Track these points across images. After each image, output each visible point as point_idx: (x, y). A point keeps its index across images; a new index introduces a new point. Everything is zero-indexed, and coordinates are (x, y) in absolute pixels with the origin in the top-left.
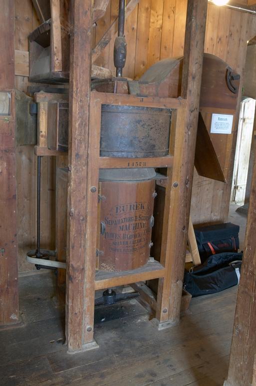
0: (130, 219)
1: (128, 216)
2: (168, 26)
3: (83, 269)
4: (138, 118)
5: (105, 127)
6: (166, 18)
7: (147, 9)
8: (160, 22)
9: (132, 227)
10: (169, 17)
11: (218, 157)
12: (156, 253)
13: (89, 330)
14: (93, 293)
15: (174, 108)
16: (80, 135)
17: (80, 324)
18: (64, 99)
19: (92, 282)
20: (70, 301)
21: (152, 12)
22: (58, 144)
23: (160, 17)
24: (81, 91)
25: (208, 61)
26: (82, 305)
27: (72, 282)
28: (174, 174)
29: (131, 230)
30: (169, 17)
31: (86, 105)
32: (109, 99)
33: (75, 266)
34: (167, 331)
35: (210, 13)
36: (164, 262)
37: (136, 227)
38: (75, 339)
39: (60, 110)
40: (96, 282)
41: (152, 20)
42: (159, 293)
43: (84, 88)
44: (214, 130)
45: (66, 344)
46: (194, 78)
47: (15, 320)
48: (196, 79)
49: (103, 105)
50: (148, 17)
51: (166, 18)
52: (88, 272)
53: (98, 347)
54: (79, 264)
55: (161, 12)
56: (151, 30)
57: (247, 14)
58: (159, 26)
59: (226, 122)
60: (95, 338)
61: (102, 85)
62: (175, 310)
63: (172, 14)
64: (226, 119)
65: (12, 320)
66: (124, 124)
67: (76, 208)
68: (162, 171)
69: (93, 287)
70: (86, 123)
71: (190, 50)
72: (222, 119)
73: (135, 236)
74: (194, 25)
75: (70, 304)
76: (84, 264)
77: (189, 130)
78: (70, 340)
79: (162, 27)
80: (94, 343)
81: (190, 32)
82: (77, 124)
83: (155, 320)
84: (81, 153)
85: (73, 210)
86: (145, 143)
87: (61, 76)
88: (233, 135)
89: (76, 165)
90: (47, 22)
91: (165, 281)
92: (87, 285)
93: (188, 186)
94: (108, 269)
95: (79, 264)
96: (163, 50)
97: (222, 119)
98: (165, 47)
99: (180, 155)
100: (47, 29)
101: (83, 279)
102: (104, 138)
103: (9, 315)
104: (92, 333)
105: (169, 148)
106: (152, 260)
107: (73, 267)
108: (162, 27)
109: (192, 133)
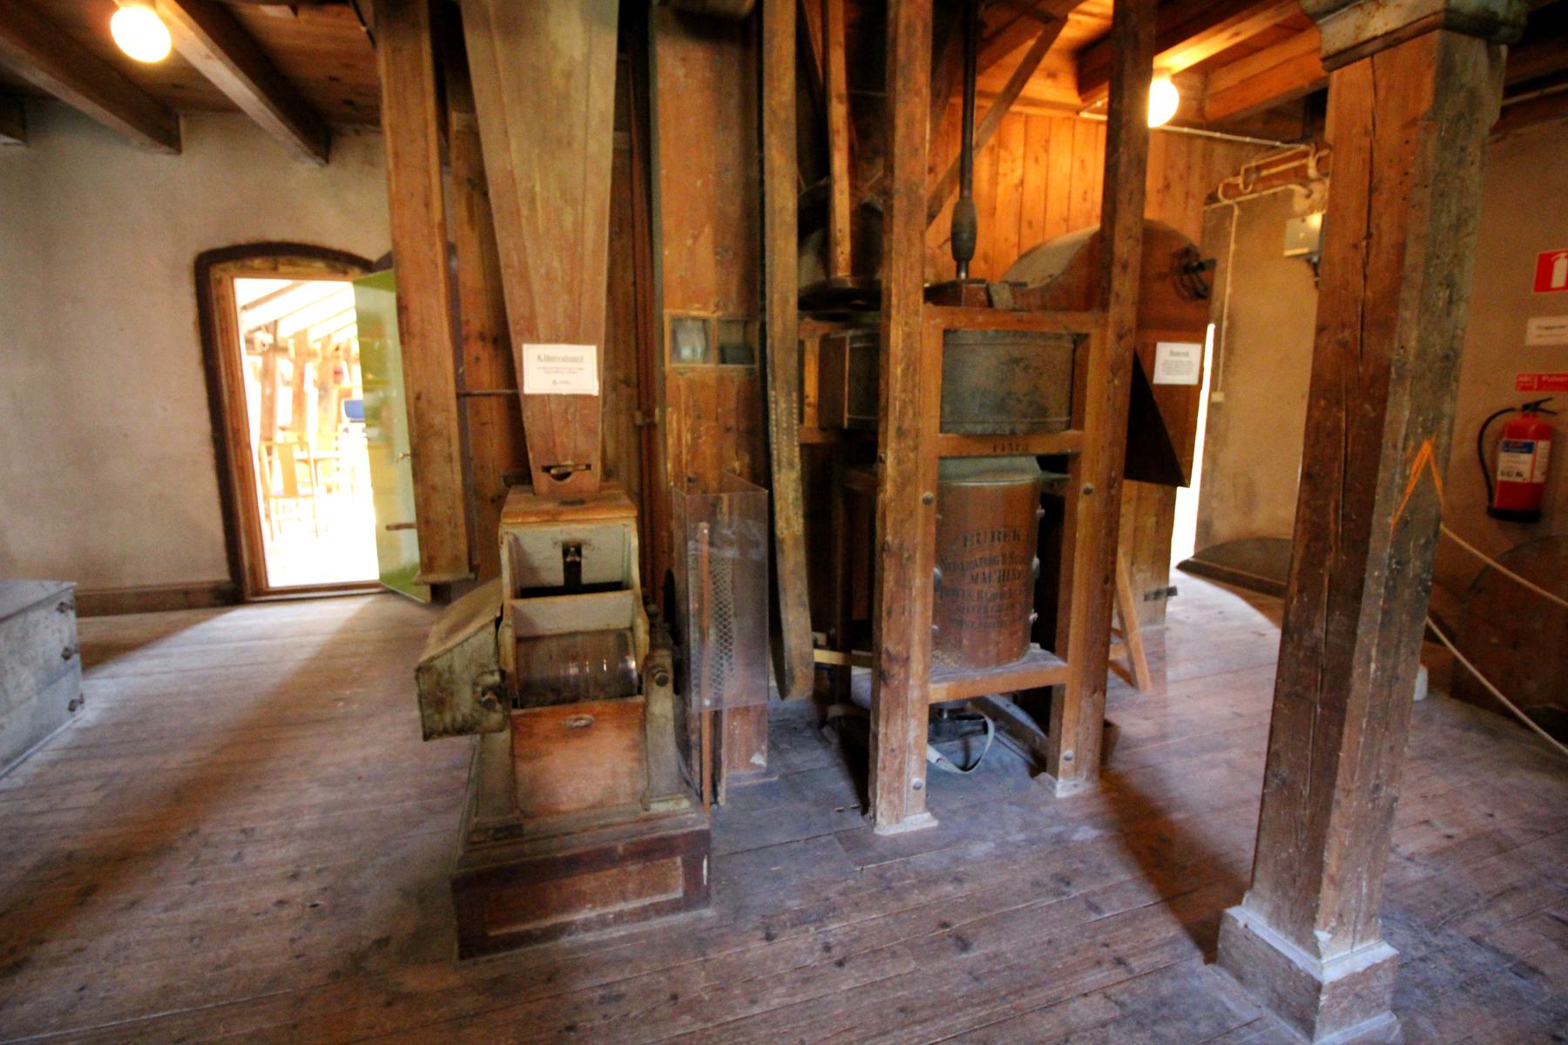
0: (992, 561)
1: (987, 554)
2: (1034, 179)
3: (908, 659)
4: (1016, 354)
5: (949, 376)
6: (1030, 163)
7: (992, 148)
8: (1019, 172)
9: (995, 577)
10: (1037, 160)
11: (1171, 433)
12: (1047, 634)
13: (917, 788)
14: (926, 709)
15: (1084, 331)
16: (904, 390)
17: (900, 773)
18: (639, 760)
19: (924, 686)
20: (882, 723)
21: (1002, 153)
22: (846, 415)
23: (1019, 162)
24: (907, 305)
25: (1151, 235)
26: (905, 733)
27: (887, 685)
28: (1085, 467)
29: (995, 583)
30: (1037, 160)
31: (911, 329)
32: (958, 317)
33: (892, 650)
34: (1074, 799)
35: (1146, 140)
36: (1066, 650)
37: (1004, 577)
38: (891, 803)
39: (852, 350)
40: (932, 687)
41: (1001, 170)
42: (1053, 723)
43: (912, 297)
44: (1162, 376)
45: (871, 813)
46: (1125, 267)
47: (759, 767)
48: (1130, 270)
49: (946, 332)
50: (995, 164)
51: (1030, 163)
52: (916, 666)
53: (935, 823)
54: (899, 648)
55: (1019, 152)
56: (1000, 190)
57: (1199, 143)
58: (1016, 181)
59: (1185, 359)
60: (929, 807)
61: (938, 294)
62: (1090, 756)
63: (1042, 155)
64: (1187, 354)
65: (753, 766)
66: (983, 366)
67: (895, 533)
68: (1050, 463)
69: (924, 697)
70: (912, 367)
71: (1114, 210)
72: (1178, 354)
73: (1002, 596)
74: (1124, 159)
75: (882, 730)
76: (908, 650)
77: (1115, 375)
78: (882, 804)
79: (1022, 183)
80: (927, 815)
81: (1115, 175)
82: (899, 371)
83: (1045, 776)
84: (906, 426)
85: (889, 538)
86: (1030, 404)
87: (850, 285)
88: (514, 339)
89: (897, 451)
90: (822, 183)
91: (1068, 692)
92: (914, 694)
93: (1113, 492)
94: (949, 662)
95: (899, 648)
96: (1025, 230)
97: (1178, 354)
98: (1030, 223)
99: (1096, 438)
100: (825, 673)
101: (907, 679)
102: (950, 397)
103: (749, 755)
104: (923, 792)
105: (1075, 417)
106: (1035, 648)
107: (888, 653)
108: (1022, 183)
109: (1122, 383)
